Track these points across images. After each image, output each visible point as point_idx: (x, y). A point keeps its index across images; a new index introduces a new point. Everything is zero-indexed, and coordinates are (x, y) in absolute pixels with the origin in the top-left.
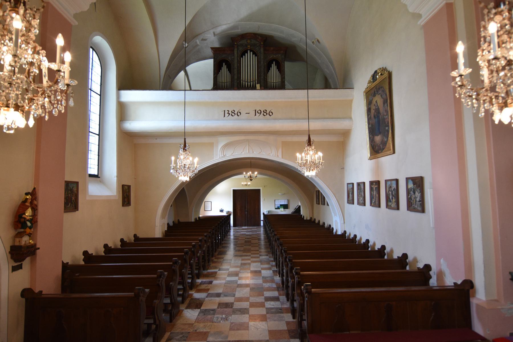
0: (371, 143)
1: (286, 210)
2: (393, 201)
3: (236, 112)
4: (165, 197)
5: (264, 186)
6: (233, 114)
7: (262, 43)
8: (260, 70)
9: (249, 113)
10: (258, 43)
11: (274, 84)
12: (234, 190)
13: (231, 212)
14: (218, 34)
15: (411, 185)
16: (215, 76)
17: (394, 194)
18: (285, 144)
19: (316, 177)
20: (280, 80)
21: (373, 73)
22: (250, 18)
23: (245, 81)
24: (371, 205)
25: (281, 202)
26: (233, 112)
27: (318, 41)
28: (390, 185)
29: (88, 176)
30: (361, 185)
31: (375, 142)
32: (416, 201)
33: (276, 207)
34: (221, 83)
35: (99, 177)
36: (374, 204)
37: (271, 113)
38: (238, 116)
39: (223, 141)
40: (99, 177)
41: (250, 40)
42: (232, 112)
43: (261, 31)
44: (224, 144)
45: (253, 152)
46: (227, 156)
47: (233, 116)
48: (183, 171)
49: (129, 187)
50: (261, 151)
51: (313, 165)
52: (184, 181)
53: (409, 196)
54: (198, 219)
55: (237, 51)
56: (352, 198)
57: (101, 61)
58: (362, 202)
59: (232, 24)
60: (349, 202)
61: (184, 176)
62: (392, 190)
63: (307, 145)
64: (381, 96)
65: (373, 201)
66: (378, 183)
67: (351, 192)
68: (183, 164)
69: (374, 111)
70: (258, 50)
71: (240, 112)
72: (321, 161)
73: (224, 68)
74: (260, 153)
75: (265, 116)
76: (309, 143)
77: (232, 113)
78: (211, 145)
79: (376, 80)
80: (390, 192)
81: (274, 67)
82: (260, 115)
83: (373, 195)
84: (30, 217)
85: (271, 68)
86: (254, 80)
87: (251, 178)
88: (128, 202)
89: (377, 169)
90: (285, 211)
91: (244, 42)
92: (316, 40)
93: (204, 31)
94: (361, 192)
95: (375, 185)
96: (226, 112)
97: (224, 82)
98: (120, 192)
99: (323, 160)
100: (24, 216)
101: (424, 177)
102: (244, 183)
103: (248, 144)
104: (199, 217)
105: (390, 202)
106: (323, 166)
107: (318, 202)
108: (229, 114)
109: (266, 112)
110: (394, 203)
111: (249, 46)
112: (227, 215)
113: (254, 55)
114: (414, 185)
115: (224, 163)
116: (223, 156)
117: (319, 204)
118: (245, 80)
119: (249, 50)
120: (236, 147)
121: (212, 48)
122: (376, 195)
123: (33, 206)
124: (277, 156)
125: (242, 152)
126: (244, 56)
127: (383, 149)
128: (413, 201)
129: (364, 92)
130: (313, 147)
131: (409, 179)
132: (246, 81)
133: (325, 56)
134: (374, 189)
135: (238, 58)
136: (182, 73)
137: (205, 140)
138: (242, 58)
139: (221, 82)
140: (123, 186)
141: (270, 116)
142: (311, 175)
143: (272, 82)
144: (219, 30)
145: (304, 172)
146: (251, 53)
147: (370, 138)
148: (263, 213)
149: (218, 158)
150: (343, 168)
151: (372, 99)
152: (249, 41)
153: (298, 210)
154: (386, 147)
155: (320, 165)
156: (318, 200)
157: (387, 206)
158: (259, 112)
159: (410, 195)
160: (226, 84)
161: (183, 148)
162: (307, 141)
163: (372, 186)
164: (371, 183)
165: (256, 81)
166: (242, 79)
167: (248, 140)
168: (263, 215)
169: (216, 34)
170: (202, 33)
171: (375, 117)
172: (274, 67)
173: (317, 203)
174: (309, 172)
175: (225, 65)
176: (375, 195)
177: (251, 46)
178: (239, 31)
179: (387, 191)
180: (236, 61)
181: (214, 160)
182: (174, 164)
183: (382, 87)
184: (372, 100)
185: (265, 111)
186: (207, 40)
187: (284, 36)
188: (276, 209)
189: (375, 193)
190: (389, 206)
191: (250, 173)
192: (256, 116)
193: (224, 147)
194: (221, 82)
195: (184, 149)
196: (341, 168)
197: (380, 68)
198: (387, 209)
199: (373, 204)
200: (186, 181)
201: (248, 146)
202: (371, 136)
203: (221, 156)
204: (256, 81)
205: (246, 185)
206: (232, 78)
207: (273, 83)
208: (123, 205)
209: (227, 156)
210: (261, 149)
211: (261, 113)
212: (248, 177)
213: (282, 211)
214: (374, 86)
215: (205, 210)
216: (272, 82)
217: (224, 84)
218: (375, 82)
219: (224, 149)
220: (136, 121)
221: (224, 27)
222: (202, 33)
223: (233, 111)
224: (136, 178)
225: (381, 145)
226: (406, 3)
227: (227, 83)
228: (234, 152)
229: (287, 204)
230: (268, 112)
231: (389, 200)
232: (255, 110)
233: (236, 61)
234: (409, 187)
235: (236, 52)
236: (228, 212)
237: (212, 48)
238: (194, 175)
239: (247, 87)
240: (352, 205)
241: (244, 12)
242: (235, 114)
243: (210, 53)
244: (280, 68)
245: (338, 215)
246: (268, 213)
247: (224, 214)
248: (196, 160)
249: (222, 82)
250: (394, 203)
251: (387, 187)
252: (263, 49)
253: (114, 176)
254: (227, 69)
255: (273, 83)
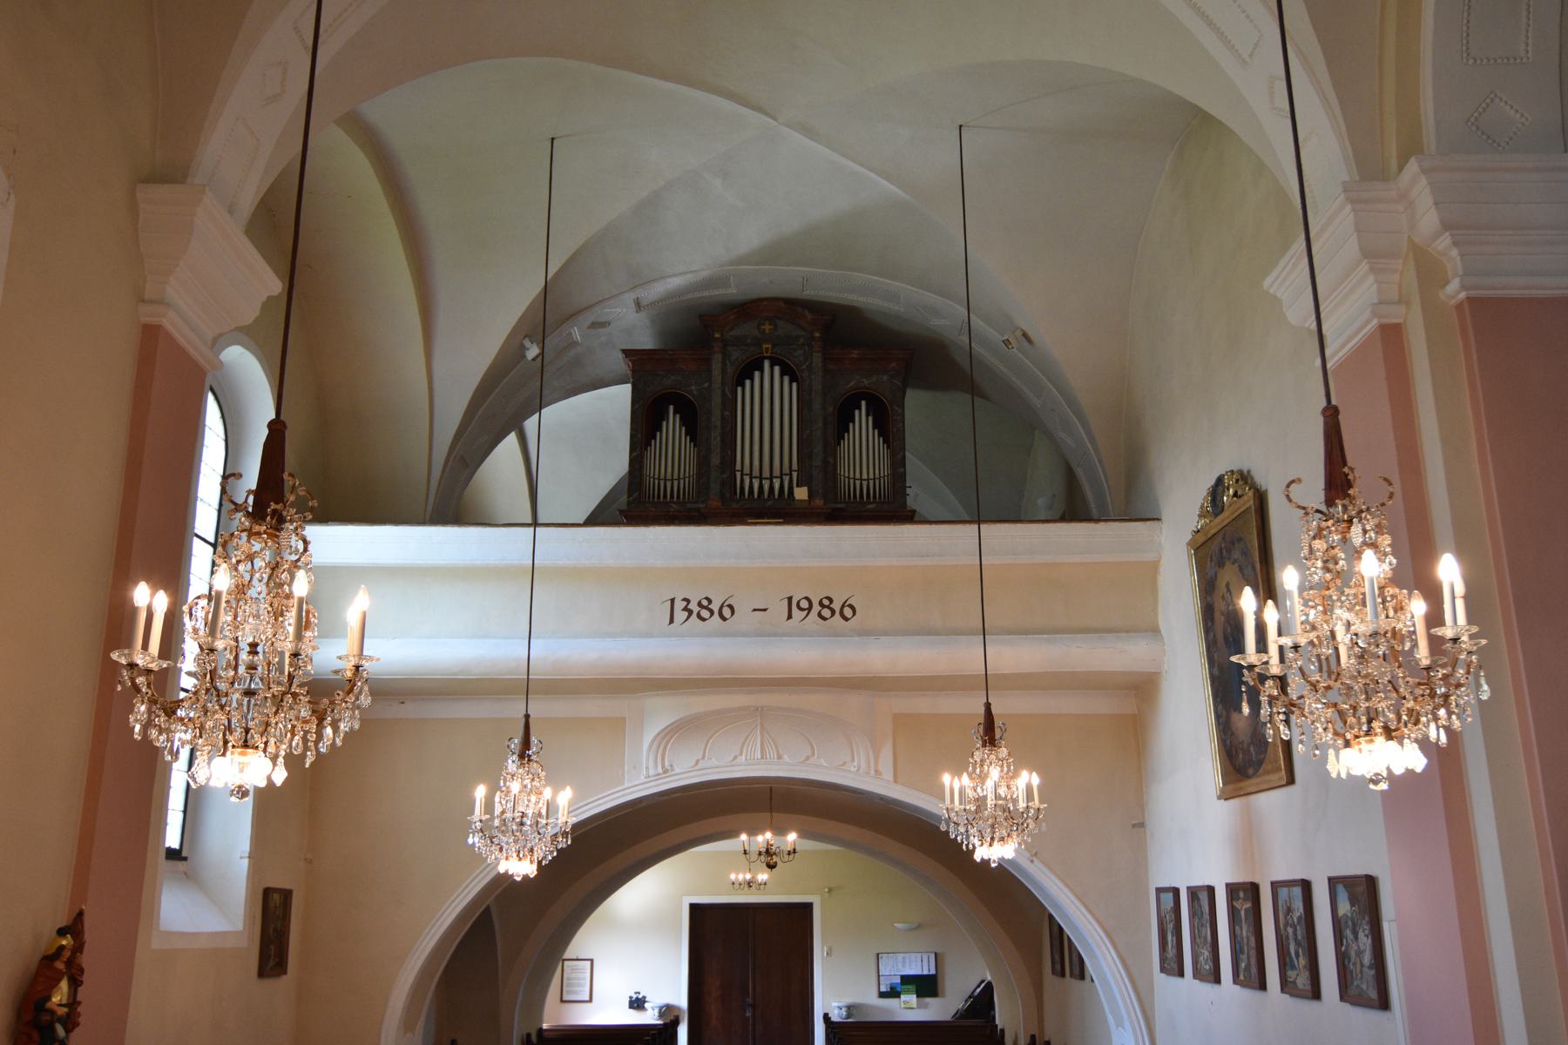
0: (1223, 737)
1: (928, 1000)
2: (1301, 965)
3: (715, 607)
4: (423, 940)
5: (830, 890)
6: (705, 614)
7: (817, 335)
8: (808, 432)
9: (765, 610)
10: (802, 333)
11: (865, 483)
12: (694, 908)
13: (679, 1009)
14: (652, 303)
15: (1344, 907)
16: (634, 454)
17: (1300, 938)
18: (905, 725)
19: (1032, 861)
20: (886, 471)
21: (1212, 482)
22: (772, 253)
23: (751, 474)
24: (1236, 980)
25: (904, 966)
26: (705, 604)
27: (1025, 335)
28: (1286, 901)
29: (163, 854)
30: (1202, 896)
31: (1233, 734)
32: (1362, 965)
33: (883, 989)
34: (657, 481)
35: (185, 859)
36: (1245, 976)
37: (847, 611)
38: (724, 619)
39: (661, 713)
40: (185, 859)
41: (770, 324)
42: (700, 604)
43: (810, 293)
44: (665, 725)
45: (780, 757)
46: (677, 770)
47: (703, 620)
48: (516, 842)
49: (287, 895)
50: (810, 753)
51: (1009, 818)
52: (519, 879)
53: (1342, 945)
54: (534, 1038)
55: (724, 364)
56: (1175, 951)
57: (227, 423)
58: (1208, 967)
59: (705, 274)
60: (1169, 967)
61: (520, 859)
62: (1295, 920)
63: (980, 742)
64: (1241, 569)
65: (1243, 965)
66: (1253, 889)
67: (1169, 927)
68: (517, 814)
69: (1223, 618)
70: (802, 359)
71: (731, 607)
72: (1036, 803)
73: (672, 425)
74: (808, 758)
75: (824, 619)
76: (990, 733)
77: (703, 610)
78: (616, 726)
79: (1223, 510)
80: (1290, 930)
81: (862, 420)
82: (807, 615)
83: (1239, 938)
84: (66, 1010)
85: (851, 425)
86: (786, 470)
87: (769, 858)
88: (277, 960)
89: (1248, 839)
90: (925, 1006)
91: (747, 329)
92: (1019, 333)
93: (601, 298)
94: (1202, 926)
95: (1244, 900)
96: (679, 605)
97: (669, 476)
98: (254, 917)
99: (1041, 802)
100: (49, 1005)
101: (1377, 878)
102: (741, 877)
103: (762, 725)
104: (541, 1030)
105: (1293, 967)
106: (1044, 824)
107: (1058, 967)
108: (690, 612)
109: (831, 606)
110: (1302, 970)
111: (770, 346)
112: (664, 1024)
113: (786, 379)
114: (1352, 905)
115: (665, 798)
116: (660, 771)
117: (1063, 975)
118: (751, 470)
119: (767, 358)
120: (713, 735)
121: (626, 352)
122: (1248, 938)
123: (73, 971)
124: (876, 771)
125: (736, 757)
126: (748, 382)
127: (1260, 763)
128: (1354, 964)
129: (1190, 544)
130: (1003, 752)
131: (1339, 882)
132: (754, 475)
133: (1057, 390)
134: (1243, 913)
135: (726, 390)
136: (512, 438)
137: (592, 707)
138: (739, 389)
139: (652, 475)
140: (267, 892)
141: (846, 619)
142: (999, 859)
143: (854, 479)
144: (657, 290)
145: (971, 847)
146: (777, 369)
147: (1218, 717)
148: (826, 1017)
149: (643, 779)
150: (1142, 825)
151: (1216, 573)
152: (767, 327)
153: (982, 1002)
154: (1267, 757)
155: (1030, 820)
156: (1057, 957)
157: (1285, 985)
158: (804, 604)
159: (1345, 941)
160: (676, 483)
161: (517, 752)
162: (982, 727)
163: (1235, 903)
164: (1232, 889)
165: (795, 474)
166: (738, 466)
167: (760, 711)
168: (824, 1025)
169: (644, 303)
170: (594, 305)
171: (1226, 639)
172: (862, 420)
173: (1054, 972)
174: (991, 845)
175: (674, 414)
176: (1245, 941)
177: (774, 345)
178: (732, 292)
179: (1282, 927)
180: (717, 400)
181: (626, 786)
182: (485, 814)
183: (1240, 540)
184: (1216, 576)
185: (826, 602)
186: (609, 324)
187: (902, 310)
188: (882, 995)
189: (1248, 931)
190: (1292, 985)
191: (768, 835)
192: (790, 620)
193: (665, 736)
194: (659, 479)
195: (522, 756)
196: (1134, 826)
197: (1232, 472)
198: (1287, 996)
199: (1242, 977)
200: (526, 878)
201: (761, 733)
202: (1220, 707)
203: (652, 772)
204: (795, 474)
205: (749, 884)
206: (703, 463)
207: (858, 482)
208: (262, 974)
209: (677, 770)
210: (812, 746)
211: (810, 609)
212: (760, 854)
213: (908, 1009)
214: (1220, 527)
215: (562, 1001)
216: (854, 479)
217: (669, 484)
218: (1221, 517)
219: (665, 748)
220: (334, 637)
221: (675, 283)
222: (594, 305)
223: (705, 603)
224: (311, 861)
225: (1252, 749)
226: (1279, 295)
227: (682, 481)
228: (703, 757)
229: (933, 972)
230: (836, 606)
231: (1288, 960)
232: (790, 599)
233: (717, 400)
234: (1341, 912)
235: (720, 365)
236: (667, 1010)
237: (626, 352)
238: (555, 854)
239: (759, 496)
240: (1178, 980)
241: (750, 236)
242: (712, 613)
243: (620, 365)
244: (888, 425)
245: (1127, 1024)
246: (849, 1016)
247: (649, 1017)
248: (565, 797)
249: (662, 476)
250: (1302, 970)
251: (1280, 908)
252: (820, 354)
253: (239, 856)
254: (684, 429)
255: (858, 482)
